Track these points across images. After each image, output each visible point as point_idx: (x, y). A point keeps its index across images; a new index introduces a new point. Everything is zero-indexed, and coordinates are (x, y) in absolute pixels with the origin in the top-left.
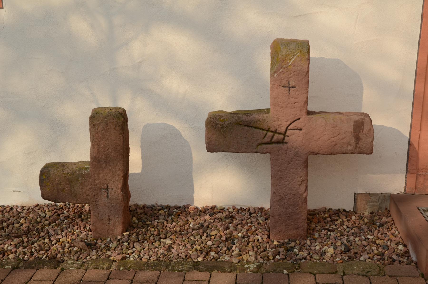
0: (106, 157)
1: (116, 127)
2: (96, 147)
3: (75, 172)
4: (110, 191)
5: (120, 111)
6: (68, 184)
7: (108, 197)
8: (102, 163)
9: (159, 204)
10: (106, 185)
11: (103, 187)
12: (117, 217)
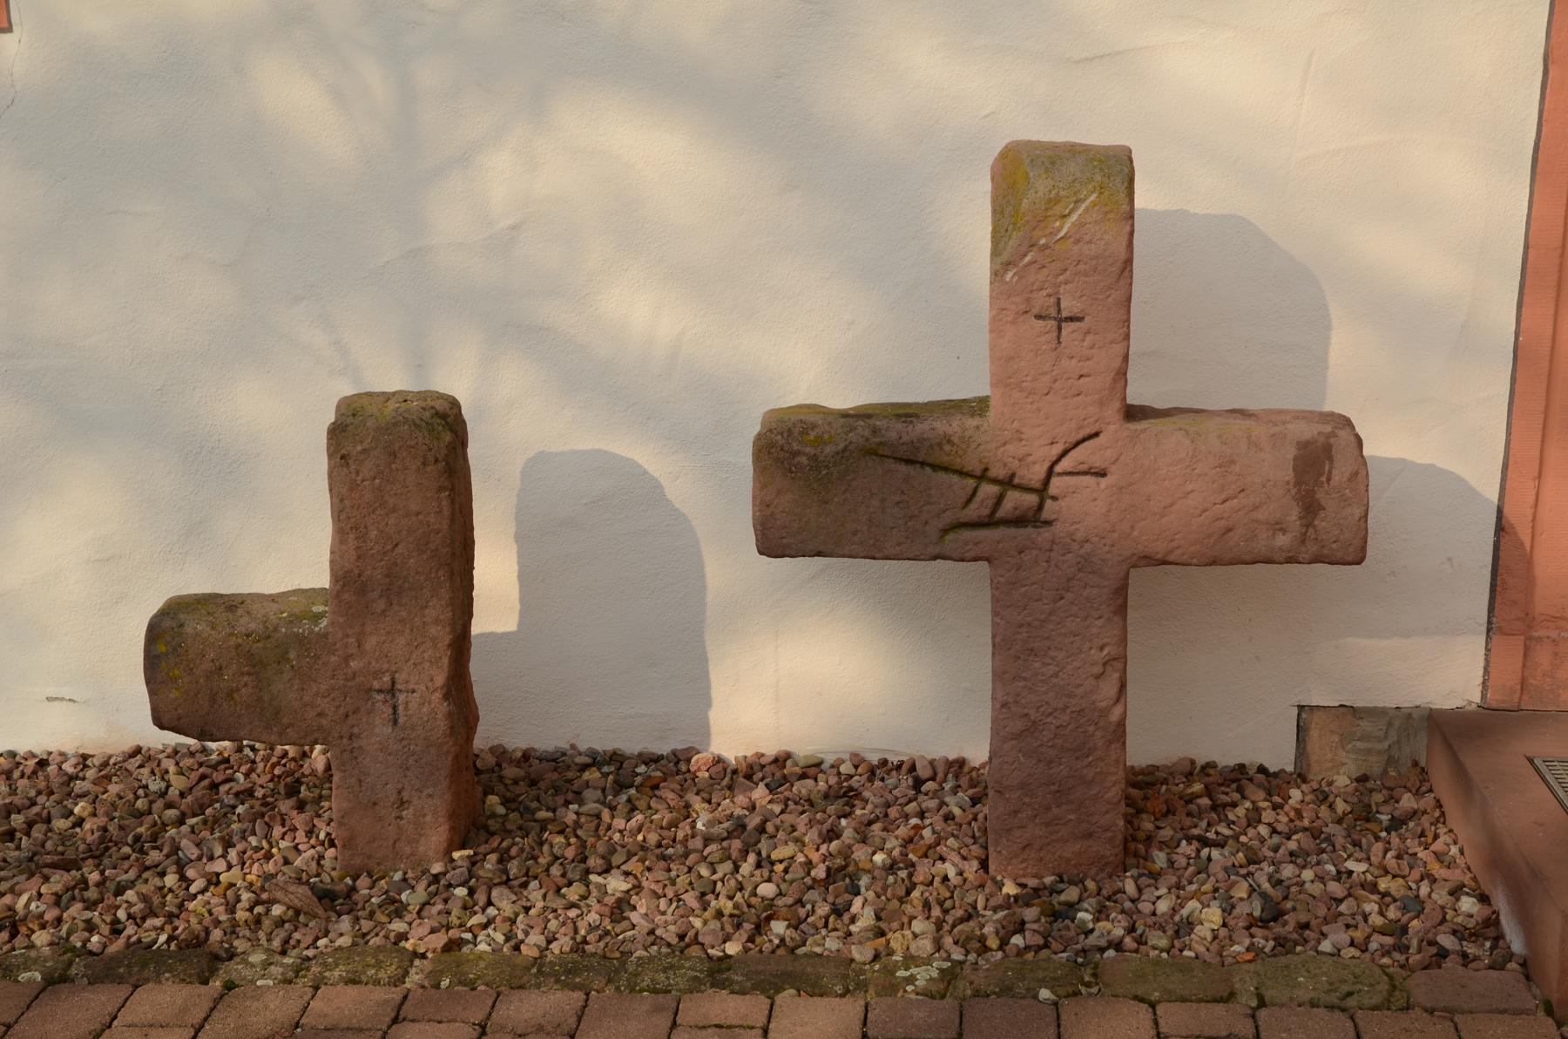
0: (387, 576)
1: (424, 464)
2: (352, 536)
3: (276, 629)
4: (401, 698)
5: (440, 405)
6: (249, 674)
7: (395, 722)
8: (375, 595)
9: (583, 747)
10: (387, 678)
11: (376, 685)
12: (430, 796)
